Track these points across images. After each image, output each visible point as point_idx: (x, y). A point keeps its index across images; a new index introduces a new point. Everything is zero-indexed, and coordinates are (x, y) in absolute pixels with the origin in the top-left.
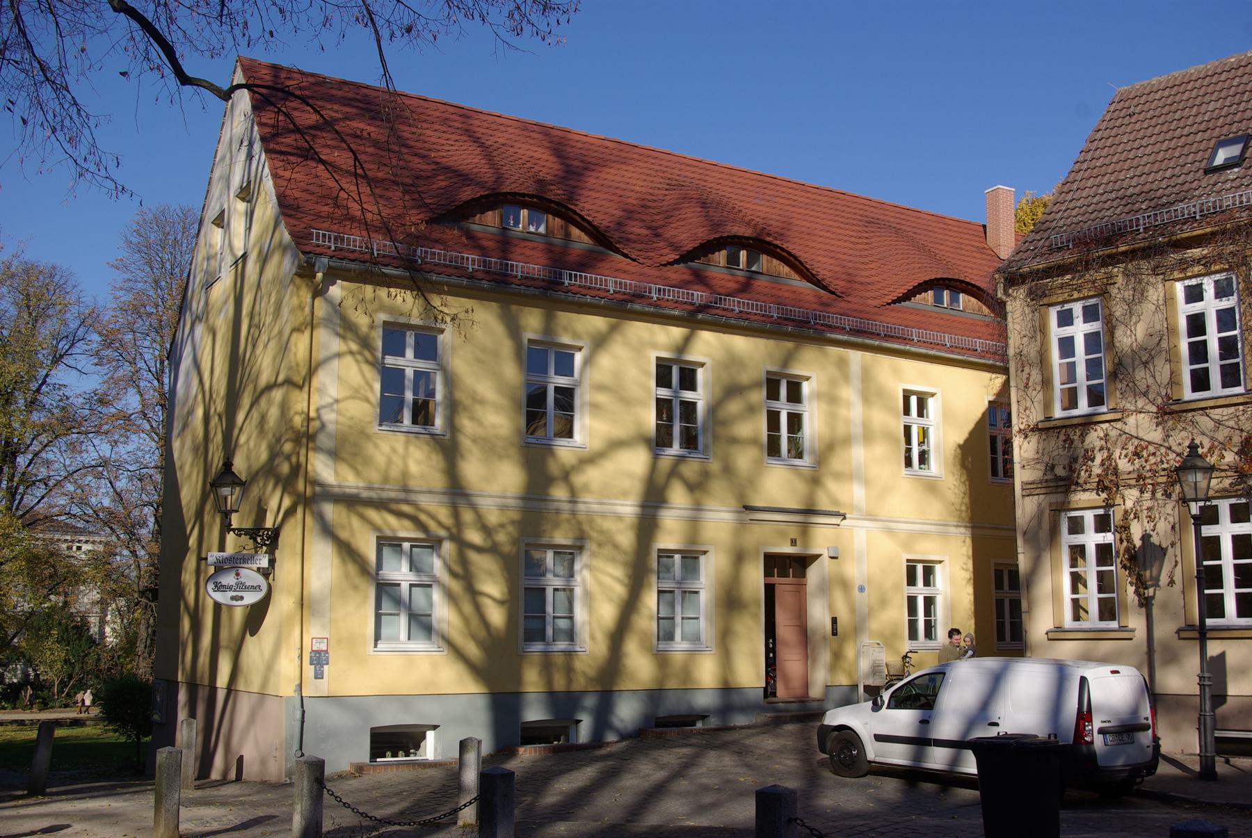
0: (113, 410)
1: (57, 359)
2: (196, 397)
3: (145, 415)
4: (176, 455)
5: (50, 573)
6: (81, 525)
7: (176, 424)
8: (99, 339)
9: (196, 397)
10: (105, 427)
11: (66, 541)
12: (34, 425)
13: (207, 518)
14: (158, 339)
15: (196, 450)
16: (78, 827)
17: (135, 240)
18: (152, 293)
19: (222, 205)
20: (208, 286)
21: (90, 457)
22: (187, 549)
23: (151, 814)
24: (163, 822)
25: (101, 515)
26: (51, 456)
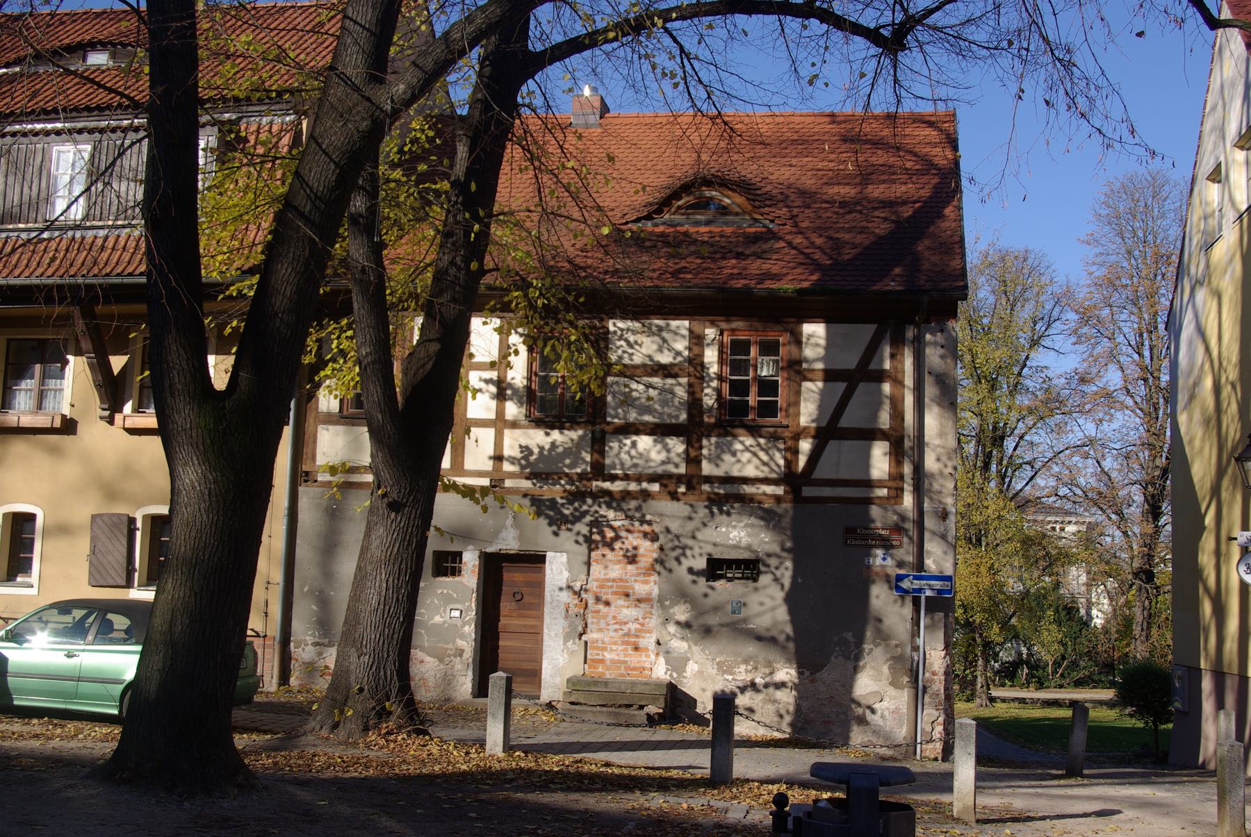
0: (1095, 388)
1: (1035, 343)
2: (1202, 366)
3: (1128, 391)
4: (1183, 430)
5: (1043, 555)
6: (1069, 506)
7: (1180, 397)
8: (1076, 317)
9: (1202, 366)
10: (1088, 407)
11: (1050, 522)
12: (1020, 409)
13: (1225, 495)
14: (1135, 311)
15: (1206, 422)
16: (1128, 814)
17: (1103, 212)
18: (1125, 264)
19: (1217, 158)
20: (1208, 247)
21: (1075, 437)
22: (1203, 528)
23: (1212, 808)
24: (1228, 820)
25: (1090, 495)
26: (1036, 439)
